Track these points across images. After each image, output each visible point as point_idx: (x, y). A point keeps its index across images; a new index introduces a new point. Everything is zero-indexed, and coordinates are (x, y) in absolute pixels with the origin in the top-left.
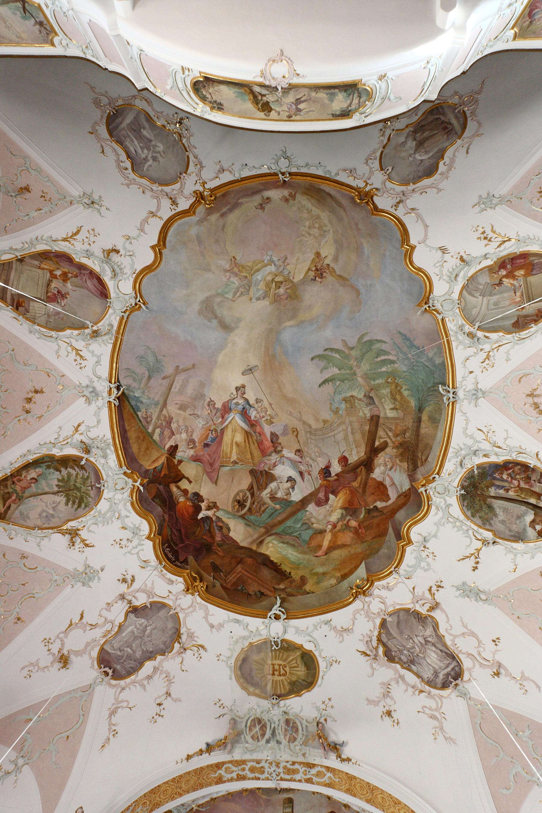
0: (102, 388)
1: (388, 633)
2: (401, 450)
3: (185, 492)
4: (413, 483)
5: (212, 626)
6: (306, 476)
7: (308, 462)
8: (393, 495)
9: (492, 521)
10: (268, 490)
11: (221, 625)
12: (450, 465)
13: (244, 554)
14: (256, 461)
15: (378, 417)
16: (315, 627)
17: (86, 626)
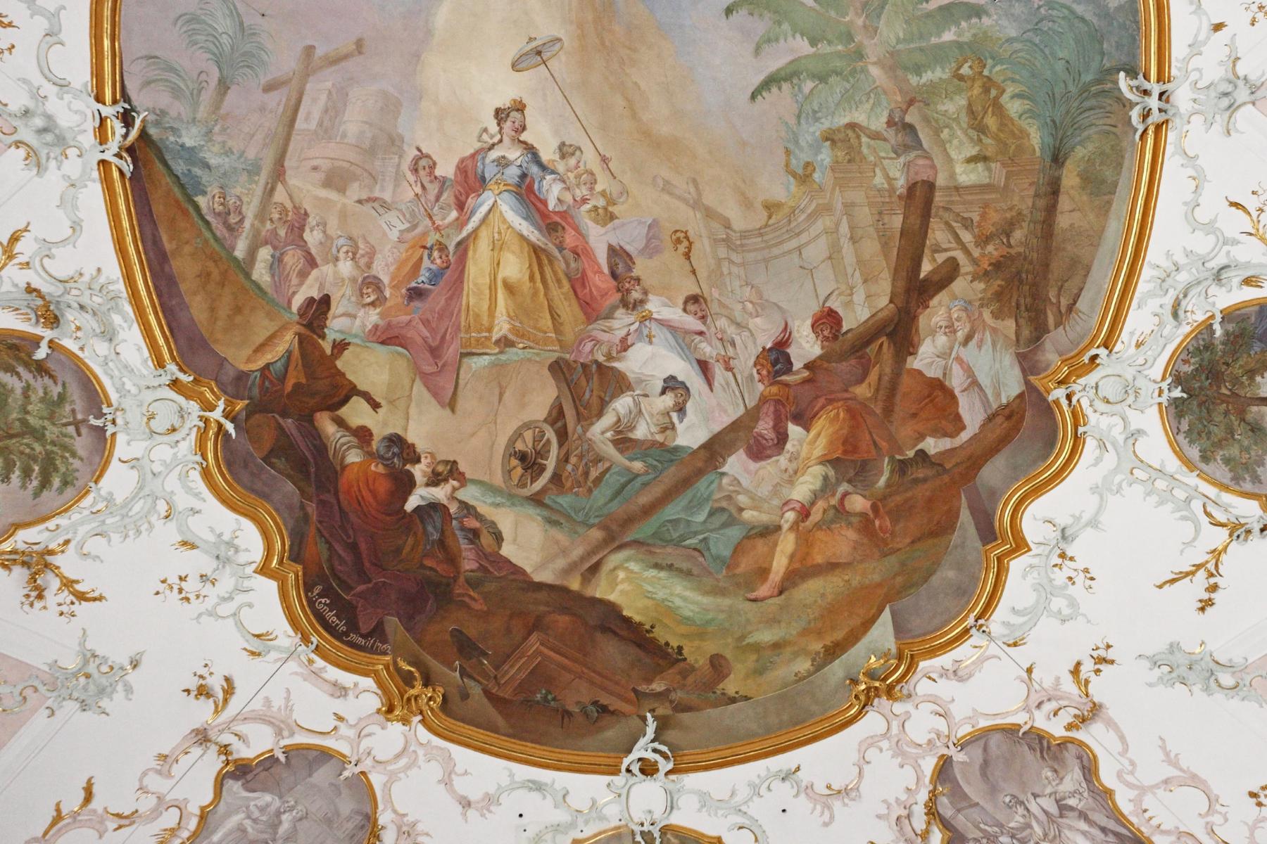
0: (77, 118)
1: (958, 794)
2: (997, 283)
3: (363, 435)
4: (1031, 378)
5: (466, 804)
6: (719, 372)
7: (723, 331)
8: (972, 415)
9: (1260, 470)
10: (608, 420)
11: (491, 801)
12: (1138, 321)
13: (547, 604)
14: (569, 336)
15: (930, 186)
16: (755, 790)
17: (102, 822)
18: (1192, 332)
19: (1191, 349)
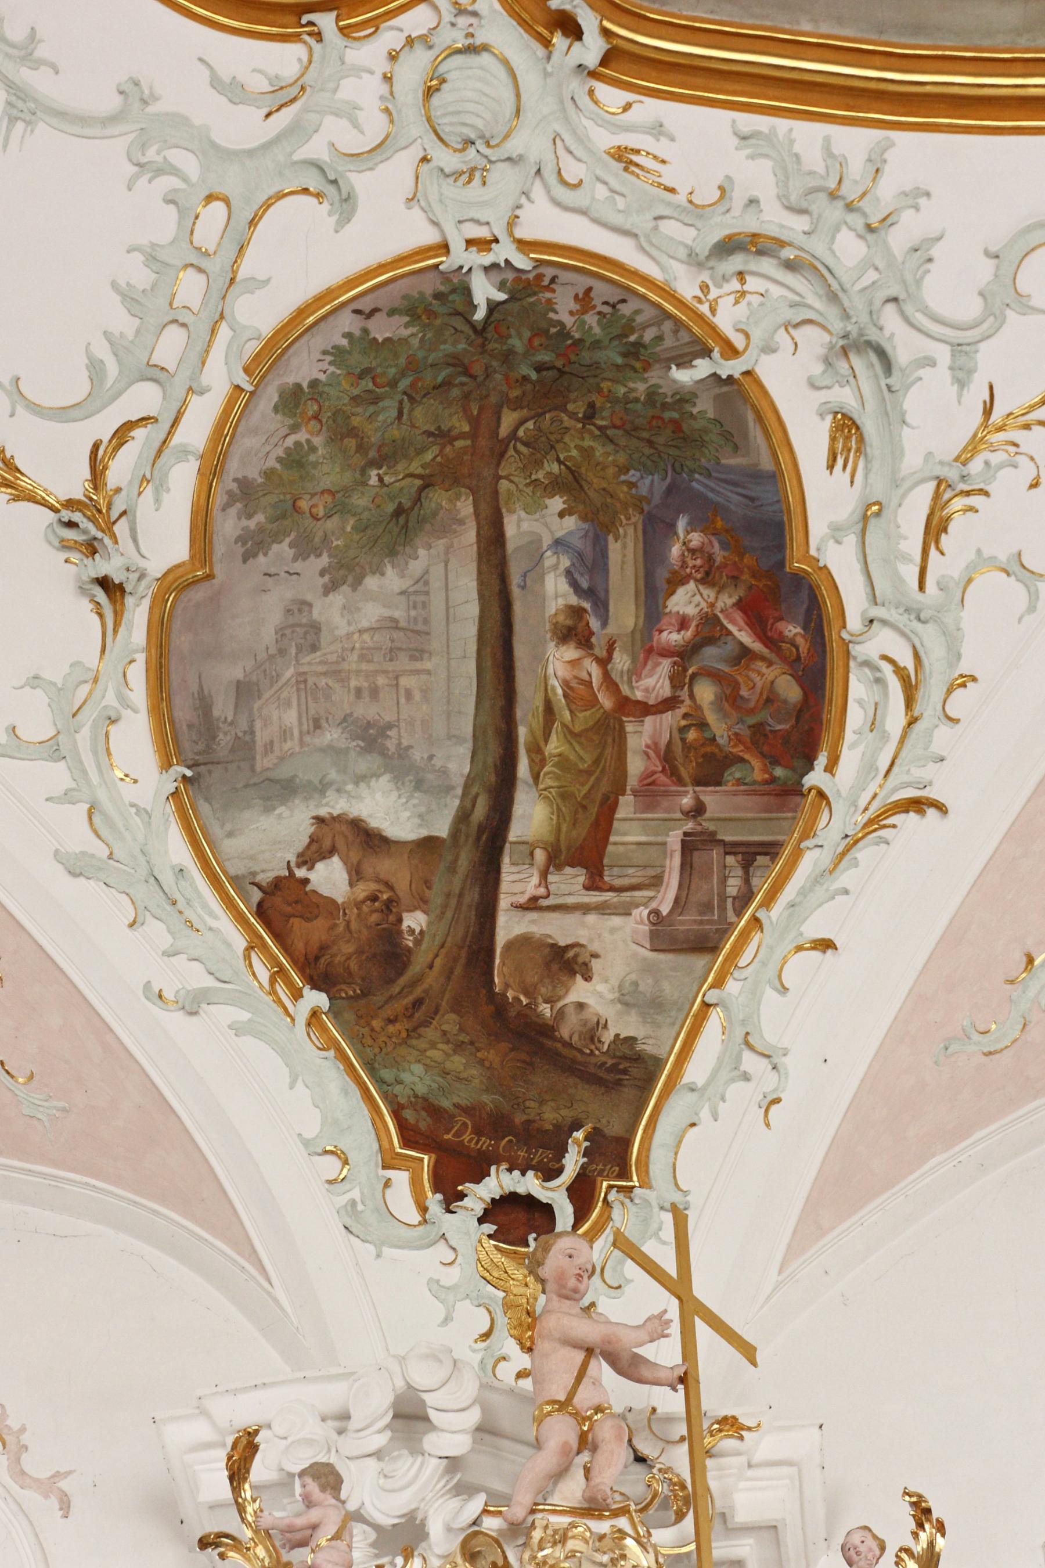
9: (283, 549)
12: (701, 144)
18: (680, 303)
19: (626, 310)
